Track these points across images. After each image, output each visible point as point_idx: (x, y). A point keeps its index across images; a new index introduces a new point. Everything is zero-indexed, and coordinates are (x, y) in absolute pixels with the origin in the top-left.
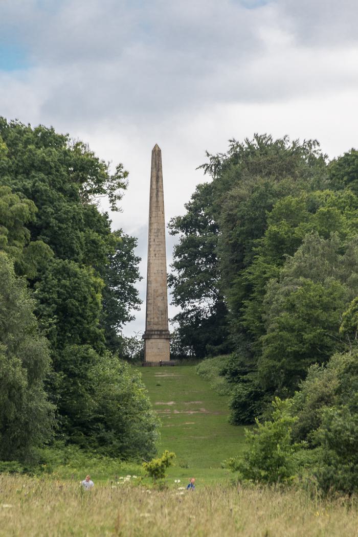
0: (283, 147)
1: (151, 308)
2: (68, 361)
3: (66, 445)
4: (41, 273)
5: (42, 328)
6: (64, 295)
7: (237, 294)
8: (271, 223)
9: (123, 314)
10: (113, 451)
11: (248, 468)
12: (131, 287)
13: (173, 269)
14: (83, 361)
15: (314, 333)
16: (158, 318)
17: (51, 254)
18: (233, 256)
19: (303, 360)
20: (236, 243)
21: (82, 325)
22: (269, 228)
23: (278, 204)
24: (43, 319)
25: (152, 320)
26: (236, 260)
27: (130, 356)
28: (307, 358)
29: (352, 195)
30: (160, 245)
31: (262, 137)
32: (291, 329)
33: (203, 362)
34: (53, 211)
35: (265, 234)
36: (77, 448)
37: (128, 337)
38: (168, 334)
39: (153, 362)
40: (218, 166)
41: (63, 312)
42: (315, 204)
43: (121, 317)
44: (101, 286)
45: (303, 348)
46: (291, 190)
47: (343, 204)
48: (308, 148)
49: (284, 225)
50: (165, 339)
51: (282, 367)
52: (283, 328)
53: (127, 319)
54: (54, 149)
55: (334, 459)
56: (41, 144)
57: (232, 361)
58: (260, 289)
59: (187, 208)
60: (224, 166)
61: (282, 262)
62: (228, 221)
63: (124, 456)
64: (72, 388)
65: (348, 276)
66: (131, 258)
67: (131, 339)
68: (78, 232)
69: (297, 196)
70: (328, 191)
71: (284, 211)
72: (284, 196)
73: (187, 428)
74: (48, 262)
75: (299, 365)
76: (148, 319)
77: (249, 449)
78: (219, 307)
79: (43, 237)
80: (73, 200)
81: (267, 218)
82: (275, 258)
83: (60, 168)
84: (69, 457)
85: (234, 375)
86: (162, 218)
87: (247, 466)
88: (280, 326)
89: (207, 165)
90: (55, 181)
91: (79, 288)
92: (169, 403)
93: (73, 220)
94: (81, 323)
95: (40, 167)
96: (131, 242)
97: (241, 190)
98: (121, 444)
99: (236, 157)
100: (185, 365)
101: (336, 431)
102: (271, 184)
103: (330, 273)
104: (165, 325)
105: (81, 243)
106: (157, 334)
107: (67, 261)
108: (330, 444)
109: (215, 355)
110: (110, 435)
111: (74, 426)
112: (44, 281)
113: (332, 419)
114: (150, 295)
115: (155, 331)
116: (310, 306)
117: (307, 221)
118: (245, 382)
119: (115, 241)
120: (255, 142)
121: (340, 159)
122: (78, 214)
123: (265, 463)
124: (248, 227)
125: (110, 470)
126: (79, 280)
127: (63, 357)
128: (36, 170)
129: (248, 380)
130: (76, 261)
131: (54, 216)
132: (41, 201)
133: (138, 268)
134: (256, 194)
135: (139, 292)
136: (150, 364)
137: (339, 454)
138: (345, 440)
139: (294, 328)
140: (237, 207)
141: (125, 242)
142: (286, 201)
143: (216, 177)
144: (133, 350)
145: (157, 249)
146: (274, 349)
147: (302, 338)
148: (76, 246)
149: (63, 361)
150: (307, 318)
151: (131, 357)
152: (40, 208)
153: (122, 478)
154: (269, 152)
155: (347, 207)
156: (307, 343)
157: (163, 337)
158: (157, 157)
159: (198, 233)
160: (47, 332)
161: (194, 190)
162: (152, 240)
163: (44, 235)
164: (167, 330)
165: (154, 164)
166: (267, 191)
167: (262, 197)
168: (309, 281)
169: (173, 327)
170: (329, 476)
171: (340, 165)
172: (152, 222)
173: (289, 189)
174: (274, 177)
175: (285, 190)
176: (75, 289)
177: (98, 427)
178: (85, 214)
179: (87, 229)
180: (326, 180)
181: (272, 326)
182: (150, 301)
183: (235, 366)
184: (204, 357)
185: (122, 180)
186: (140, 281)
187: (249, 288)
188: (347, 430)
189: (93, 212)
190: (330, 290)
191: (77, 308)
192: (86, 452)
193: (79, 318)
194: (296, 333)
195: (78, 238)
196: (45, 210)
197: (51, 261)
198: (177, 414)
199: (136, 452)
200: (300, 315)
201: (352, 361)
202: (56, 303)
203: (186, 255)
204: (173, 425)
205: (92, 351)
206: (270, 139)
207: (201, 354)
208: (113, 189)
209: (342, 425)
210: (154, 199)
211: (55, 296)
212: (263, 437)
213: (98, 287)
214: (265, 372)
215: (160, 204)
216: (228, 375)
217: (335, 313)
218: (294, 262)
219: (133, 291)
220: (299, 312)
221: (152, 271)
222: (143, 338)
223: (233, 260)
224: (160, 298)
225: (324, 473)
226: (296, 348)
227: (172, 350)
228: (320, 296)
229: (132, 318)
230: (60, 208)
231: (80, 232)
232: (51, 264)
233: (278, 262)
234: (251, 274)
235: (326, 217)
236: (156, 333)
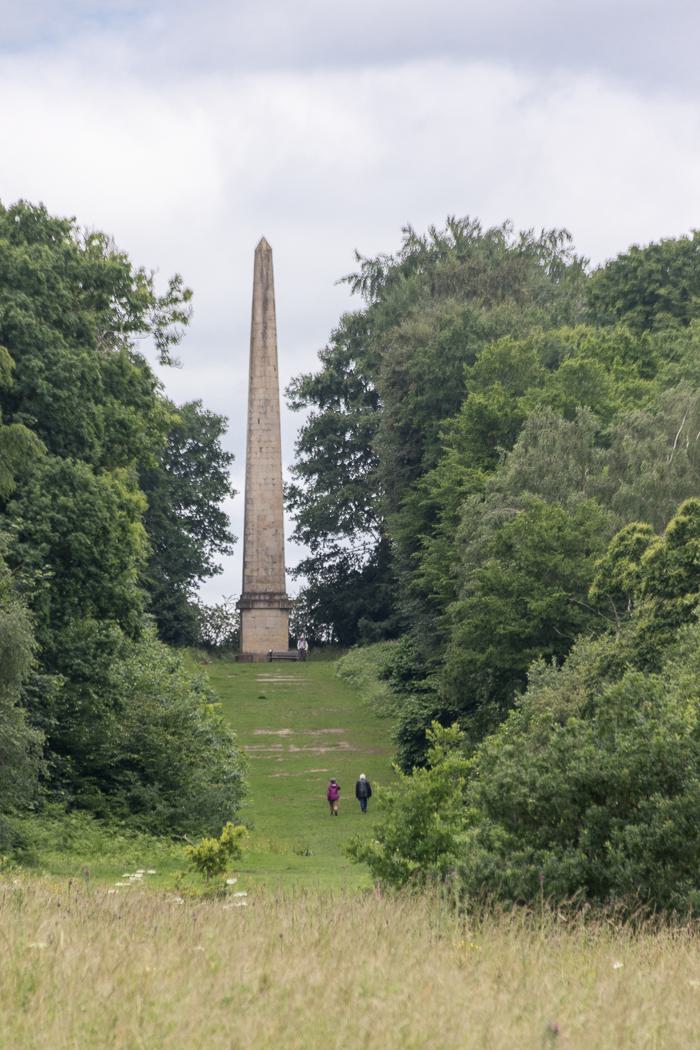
0: (502, 243)
1: (252, 550)
2: (70, 650)
3: (68, 812)
4: (21, 484)
5: (22, 589)
6: (64, 525)
7: (410, 524)
8: (474, 389)
9: (199, 561)
10: (157, 822)
11: (383, 856)
12: (216, 510)
13: (296, 476)
14: (100, 650)
15: (548, 599)
16: (266, 569)
17: (40, 448)
18: (404, 452)
19: (528, 651)
20: (408, 425)
21: (99, 582)
22: (470, 396)
23: (486, 351)
24: (26, 572)
25: (255, 574)
26: (409, 460)
27: (213, 643)
28: (536, 646)
29: (628, 334)
30: (268, 430)
31: (462, 224)
32: (504, 591)
33: (350, 652)
34: (43, 365)
35: (461, 408)
36: (89, 817)
37: (209, 606)
38: (286, 601)
39: (256, 655)
40: (377, 278)
41: (62, 556)
42: (556, 353)
43: (197, 567)
44: (139, 508)
45: (527, 627)
46: (512, 326)
47: (610, 353)
48: (549, 244)
49: (496, 392)
50: (279, 609)
51: (487, 664)
52: (489, 589)
53: (207, 572)
54: (46, 247)
55: (498, 840)
56: (21, 236)
57: (403, 652)
58: (451, 514)
59: (323, 359)
60: (391, 280)
61: (494, 464)
62: (394, 385)
63: (177, 833)
64: (80, 703)
65: (615, 489)
66: (215, 456)
67: (216, 611)
68: (92, 404)
69: (525, 337)
70: (582, 327)
71: (497, 365)
72: (497, 337)
73: (313, 780)
74: (34, 462)
75: (520, 659)
76: (248, 572)
77: (385, 821)
78: (383, 551)
79: (25, 415)
80: (83, 344)
81: (466, 378)
82: (480, 455)
83: (58, 283)
84: (73, 833)
85: (406, 678)
86: (273, 379)
87: (378, 849)
88: (483, 587)
89: (356, 276)
90: (46, 307)
91: (94, 513)
92: (280, 732)
93: (81, 382)
94: (97, 578)
95: (19, 281)
96: (216, 425)
97: (421, 325)
98: (172, 810)
99: (412, 261)
100: (320, 660)
101: (502, 786)
102: (476, 313)
103: (579, 485)
104: (279, 583)
105: (97, 426)
106: (265, 601)
107: (69, 460)
108: (489, 810)
109: (374, 640)
110: (150, 793)
111: (84, 775)
112: (25, 499)
113: (495, 762)
114: (250, 526)
115: (260, 594)
116: (541, 548)
117: (542, 384)
118: (425, 691)
119: (169, 422)
120: (449, 233)
121: (611, 265)
122: (91, 369)
123: (414, 846)
124: (430, 397)
125: (150, 858)
126: (92, 497)
127: (61, 643)
128: (11, 286)
129: (430, 688)
130: (87, 460)
131: (44, 376)
132: (20, 347)
133: (228, 473)
134: (447, 333)
135: (231, 520)
136: (250, 658)
137: (510, 829)
138: (519, 804)
139: (510, 588)
140: (410, 357)
141: (203, 425)
142: (501, 347)
143: (374, 299)
144: (220, 631)
145: (264, 438)
146: (473, 629)
147: (525, 608)
148: (87, 430)
149: (60, 651)
150: (536, 570)
151: (215, 644)
152: (18, 361)
153: (128, 875)
154: (475, 253)
155: (617, 358)
156: (535, 617)
157: (276, 605)
158: (265, 261)
159: (343, 408)
160: (30, 599)
161: (336, 324)
162: (255, 420)
163: (27, 411)
164: (283, 593)
165: (258, 275)
166: (468, 329)
167: (458, 338)
168: (537, 499)
169: (296, 586)
170: (487, 872)
171: (608, 277)
172: (255, 386)
173: (509, 323)
174: (480, 301)
175: (501, 325)
176: (84, 514)
177: (127, 779)
178: (104, 370)
179: (109, 399)
180: (580, 306)
181: (468, 586)
182: (250, 538)
183: (407, 662)
184: (353, 643)
185: (181, 307)
186: (232, 497)
187: (431, 514)
188: (523, 783)
189: (120, 367)
190: (578, 517)
191: (90, 548)
192: (106, 825)
193: (93, 569)
194: (513, 599)
195: (92, 416)
196: (27, 364)
197: (39, 460)
198: (297, 753)
199: (200, 825)
200: (522, 565)
201: (612, 652)
202: (48, 540)
203: (321, 448)
204: (286, 774)
205: (116, 632)
206: (478, 227)
207: (348, 638)
208: (162, 323)
209: (512, 775)
210: (259, 343)
211: (46, 527)
212: (410, 798)
213: (134, 510)
214: (454, 674)
215: (270, 351)
216: (395, 678)
217: (587, 560)
218: (513, 463)
219: (221, 518)
220: (520, 559)
221: (254, 481)
222: (237, 608)
223: (402, 459)
224: (270, 532)
225: (478, 867)
226: (513, 627)
227: (294, 631)
228: (560, 529)
229: (217, 570)
230: (56, 359)
231: (96, 404)
232: (38, 465)
233: (486, 464)
234: (437, 481)
235: (578, 378)
236: (262, 598)
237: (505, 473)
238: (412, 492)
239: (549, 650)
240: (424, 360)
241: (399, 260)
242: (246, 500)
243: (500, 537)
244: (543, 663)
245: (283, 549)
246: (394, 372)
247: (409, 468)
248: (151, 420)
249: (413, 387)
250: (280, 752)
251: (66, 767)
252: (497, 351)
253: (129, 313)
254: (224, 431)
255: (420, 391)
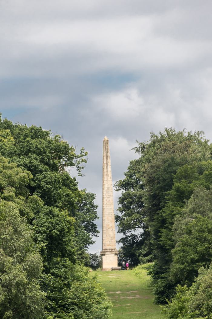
8: (176, 182)
16: (110, 241)
20: (155, 194)
21: (62, 246)
22: (175, 184)
23: (179, 170)
25: (106, 243)
37: (92, 254)
39: (107, 269)
42: (201, 169)
48: (197, 136)
49: (183, 182)
52: (185, 244)
62: (150, 181)
66: (92, 206)
67: (94, 255)
72: (183, 165)
81: (173, 178)
88: (183, 244)
92: (117, 293)
98: (87, 317)
99: (154, 142)
120: (165, 133)
134: (166, 164)
140: (155, 172)
145: (108, 200)
151: (94, 266)
158: (106, 144)
163: (38, 192)
167: (170, 165)
168: (199, 215)
182: (104, 232)
185: (84, 158)
202: (45, 232)
204: (120, 306)
218: (190, 204)
221: (105, 214)
228: (207, 225)
230: (47, 175)
233: (181, 205)
234: (165, 212)
237: (187, 208)
238: (157, 215)
239: (204, 263)
240: (159, 173)
241: (150, 142)
243: (187, 228)
244: (203, 267)
246: (150, 177)
247: (156, 207)
248: (76, 194)
249: (156, 181)
250: (117, 299)
251: (53, 305)
252: (183, 169)
253: (68, 160)
254: (95, 198)
255: (159, 183)
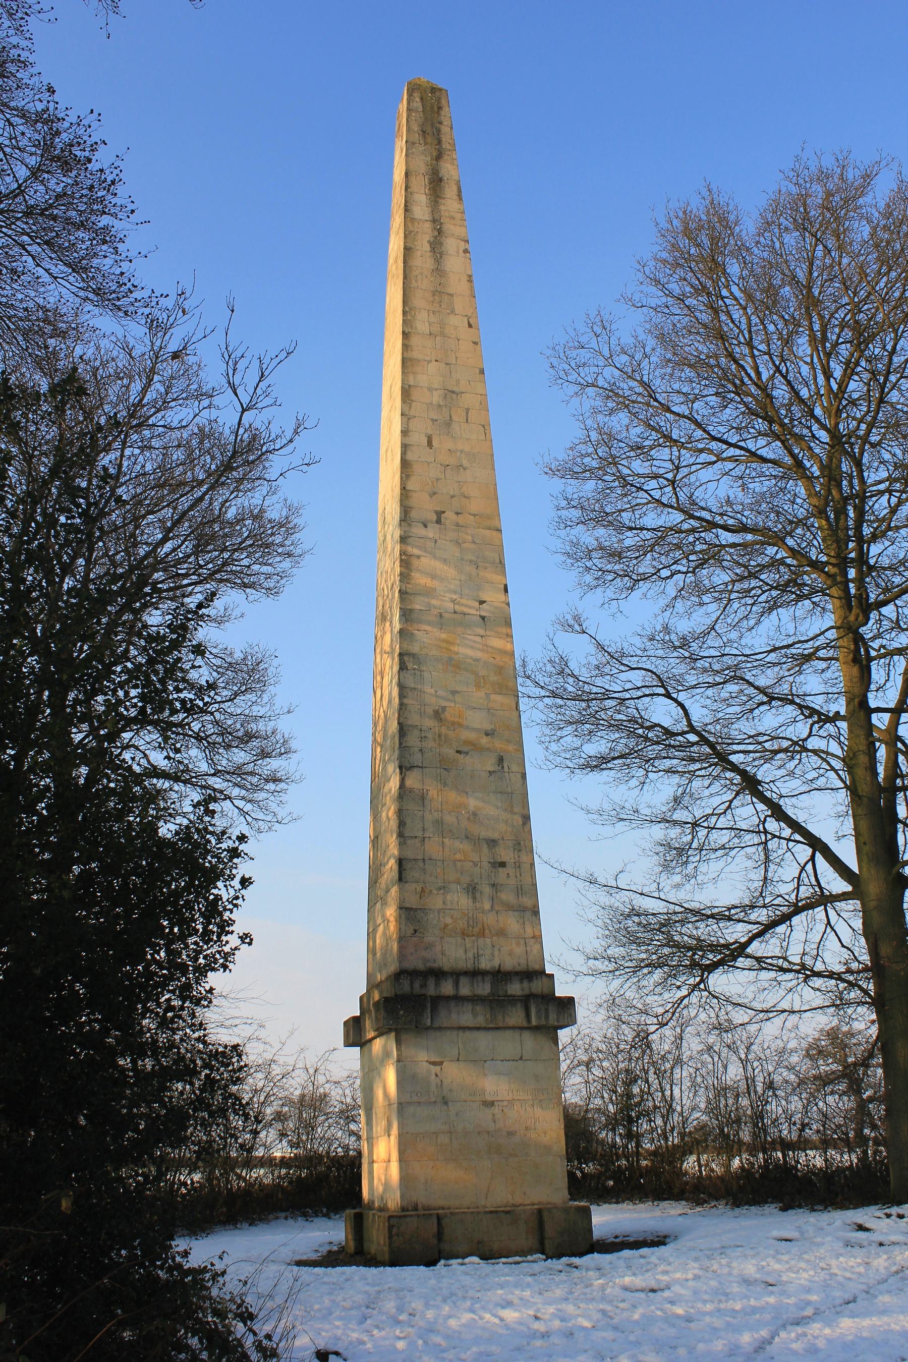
106: (475, 999)
115: (457, 975)
172: (415, 354)
213: (600, 543)
242: (404, 361)
245: (526, 818)
